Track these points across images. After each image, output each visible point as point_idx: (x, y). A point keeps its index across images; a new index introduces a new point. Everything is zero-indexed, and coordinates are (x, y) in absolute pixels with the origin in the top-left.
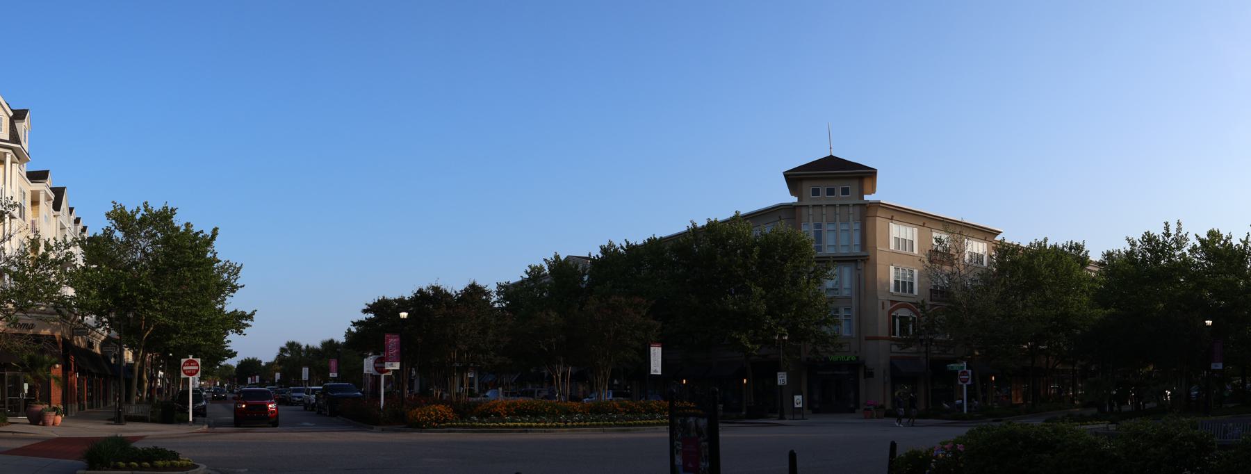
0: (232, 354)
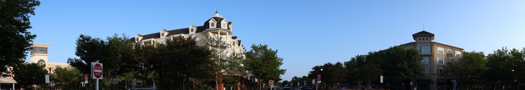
0: (281, 80)
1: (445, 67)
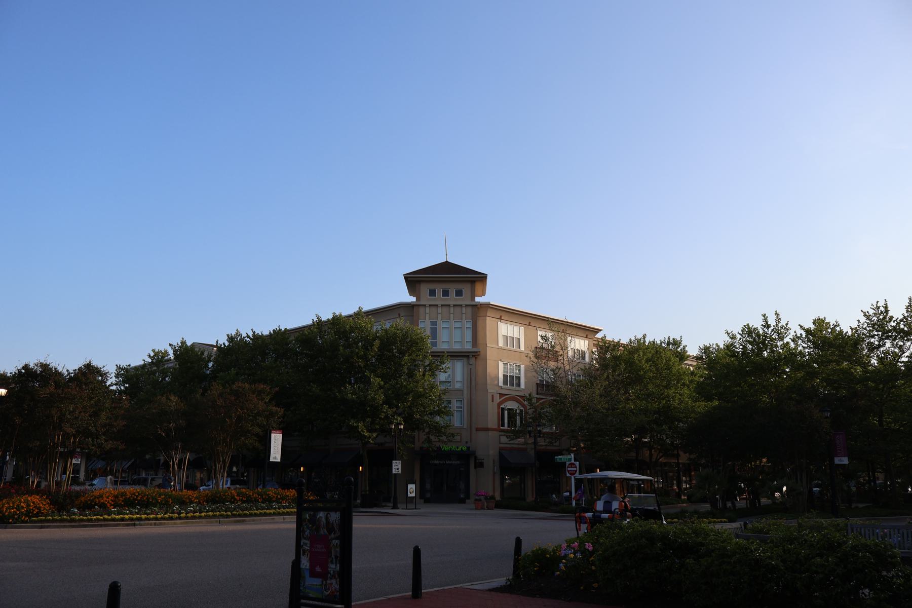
1: (529, 400)
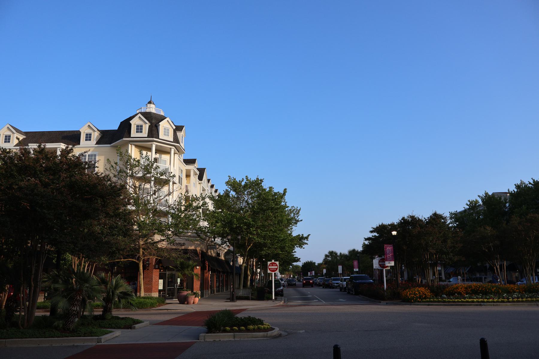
0: (298, 260)
